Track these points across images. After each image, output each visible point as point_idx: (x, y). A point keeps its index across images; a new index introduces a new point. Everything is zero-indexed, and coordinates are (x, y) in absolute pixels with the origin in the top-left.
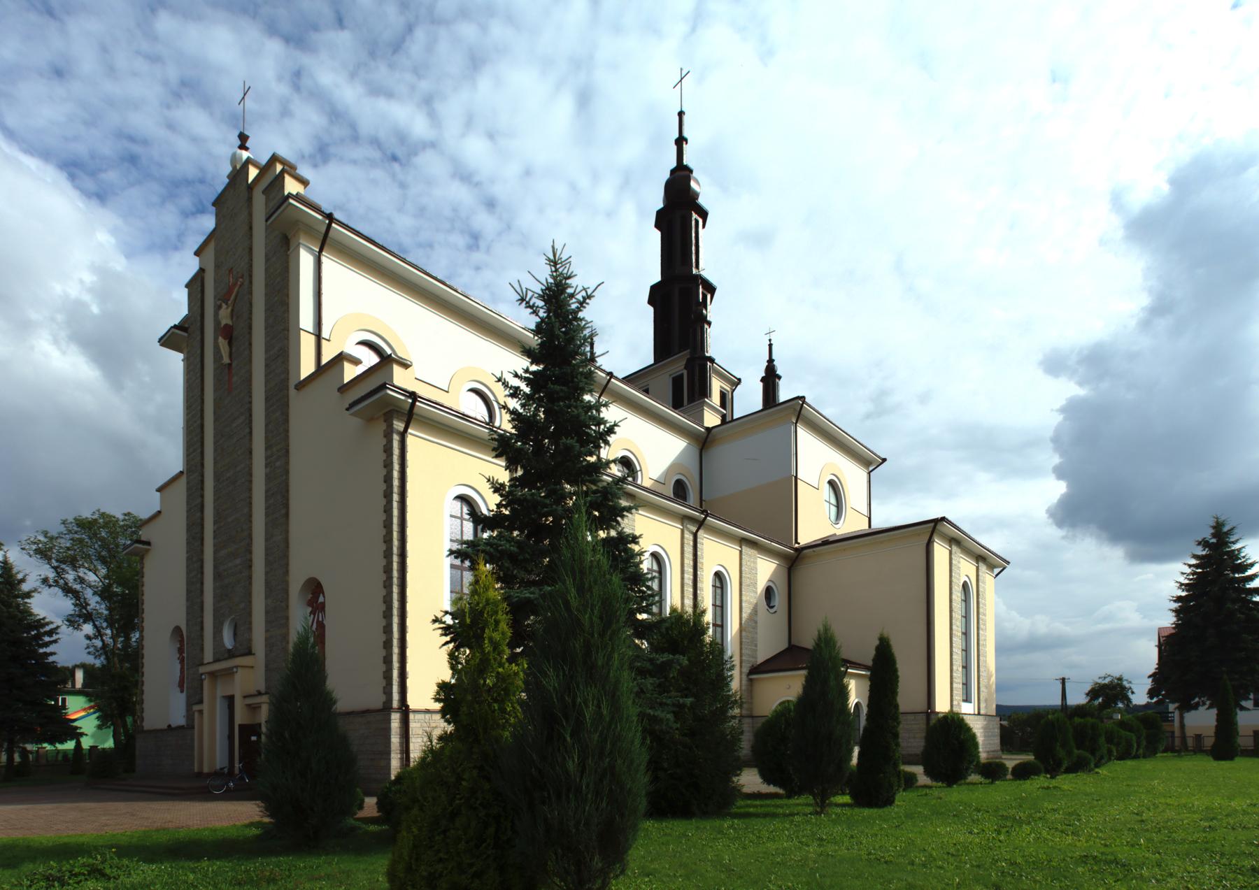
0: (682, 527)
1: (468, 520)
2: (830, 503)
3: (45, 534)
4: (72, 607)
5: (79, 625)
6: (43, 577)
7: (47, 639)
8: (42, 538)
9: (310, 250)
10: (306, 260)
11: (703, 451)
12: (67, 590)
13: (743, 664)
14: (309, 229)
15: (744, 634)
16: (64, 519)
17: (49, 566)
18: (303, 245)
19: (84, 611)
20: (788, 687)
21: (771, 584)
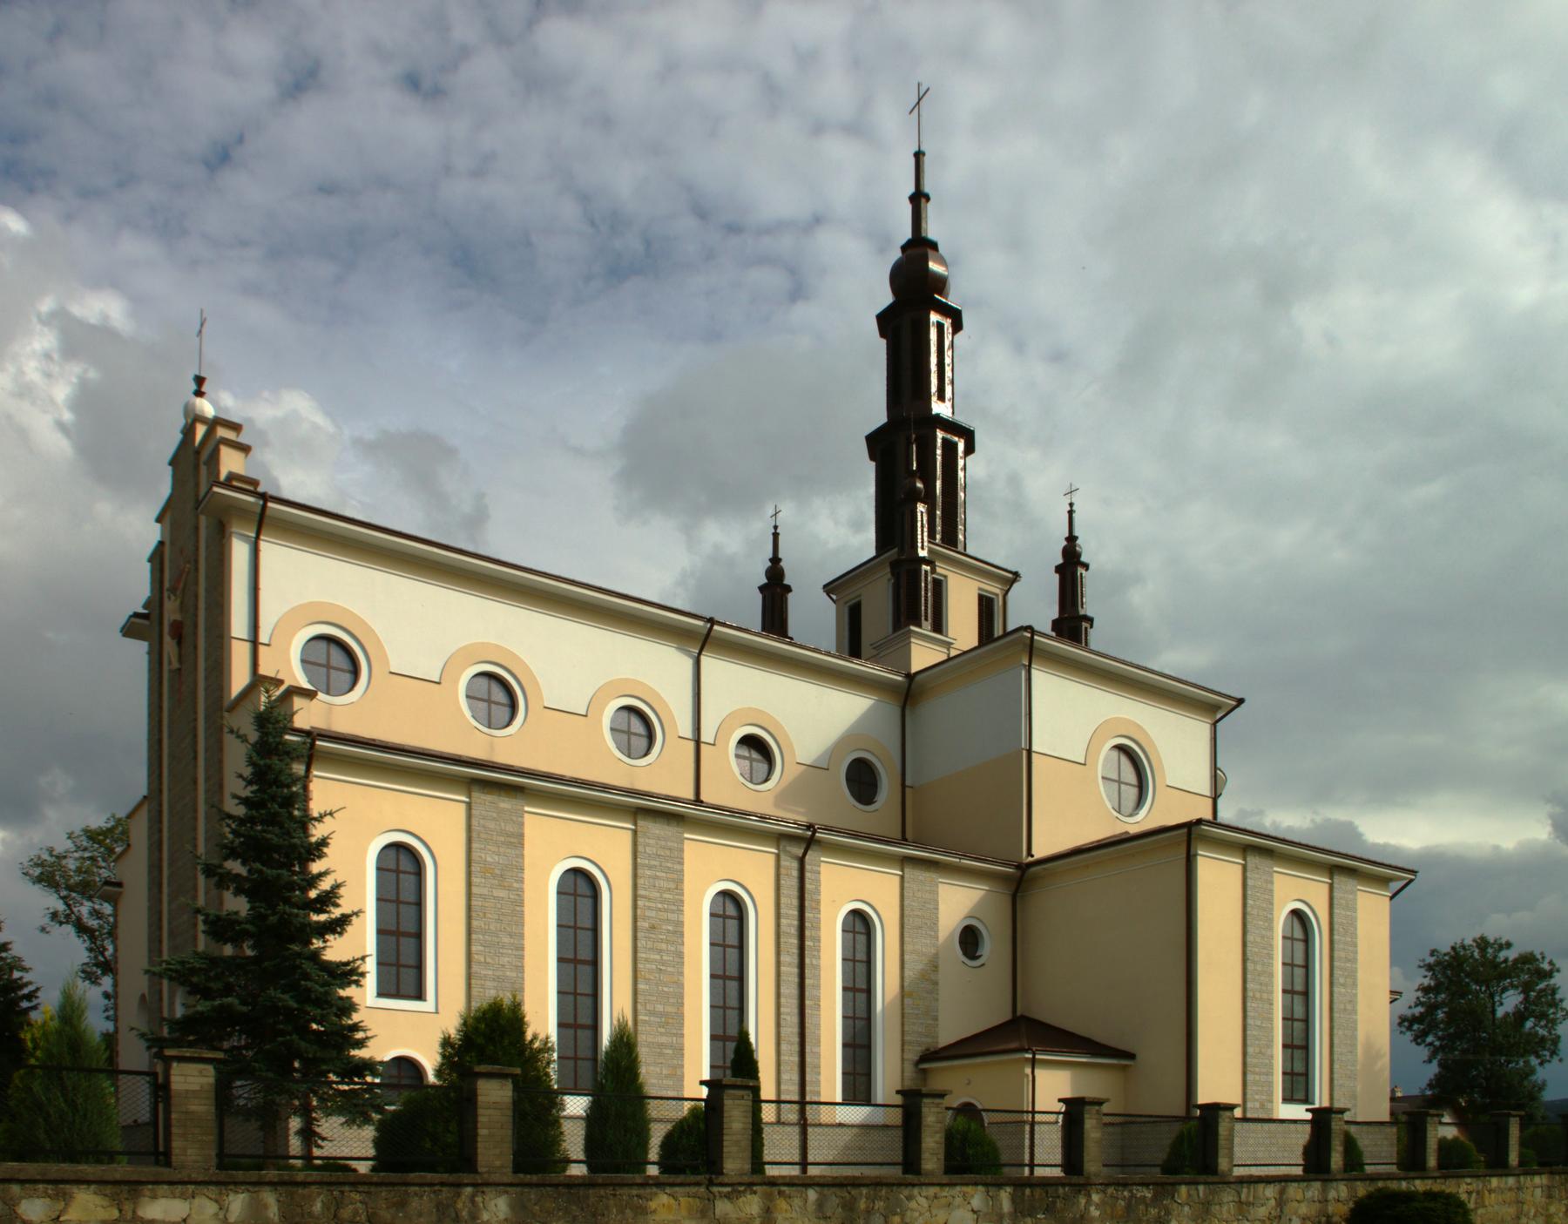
0: (776, 851)
1: (758, 761)
2: (1119, 782)
3: (51, 851)
4: (86, 954)
5: (97, 978)
6: (52, 911)
7: (25, 1004)
8: (46, 856)
9: (244, 538)
10: (239, 552)
11: (908, 707)
12: (81, 928)
13: (906, 1047)
14: (241, 511)
15: (907, 1001)
16: (69, 831)
17: (56, 896)
18: (236, 533)
19: (101, 958)
20: (967, 1082)
21: (974, 922)
